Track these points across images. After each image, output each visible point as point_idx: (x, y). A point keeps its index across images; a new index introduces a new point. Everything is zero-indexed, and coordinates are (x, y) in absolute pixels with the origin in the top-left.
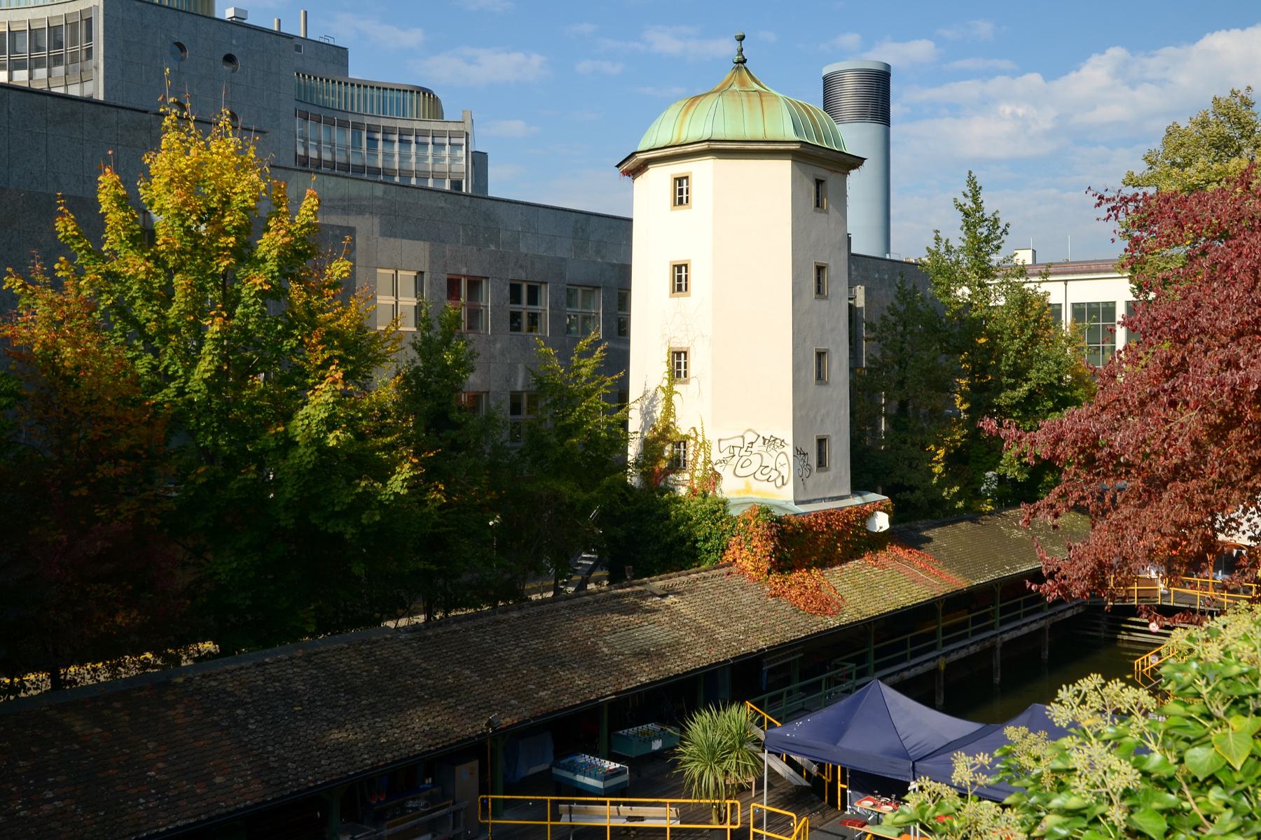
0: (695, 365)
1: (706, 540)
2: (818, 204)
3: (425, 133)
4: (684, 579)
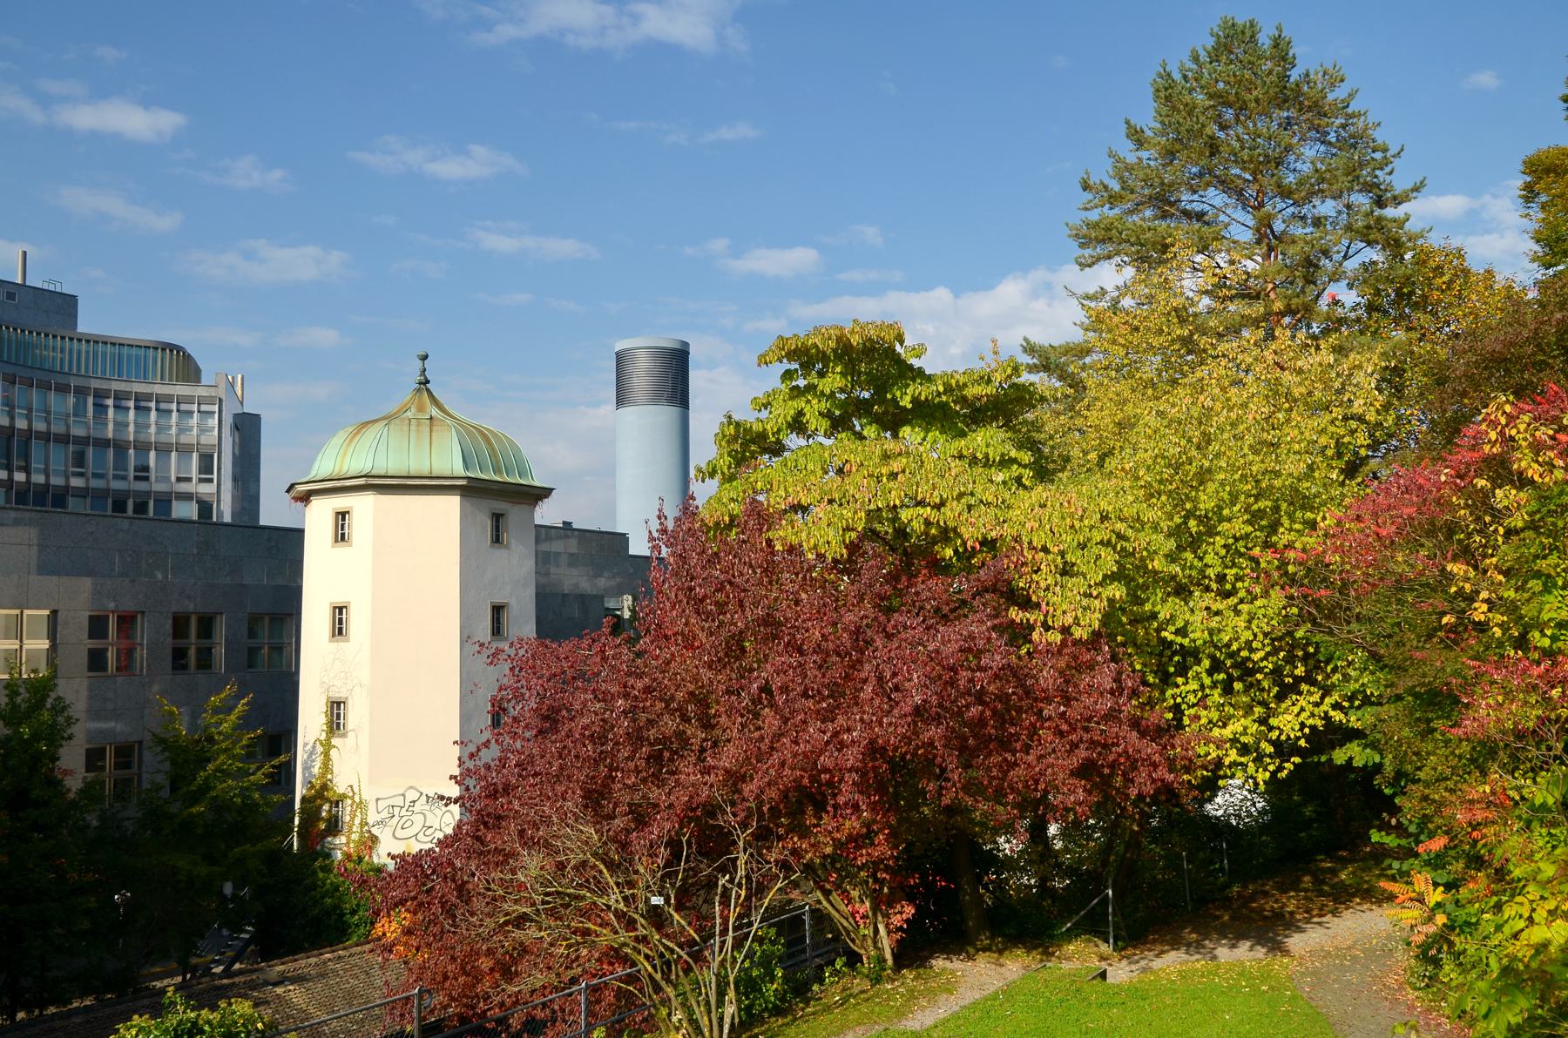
0: (354, 716)
1: (353, 912)
2: (497, 539)
3: (169, 399)
4: (313, 960)
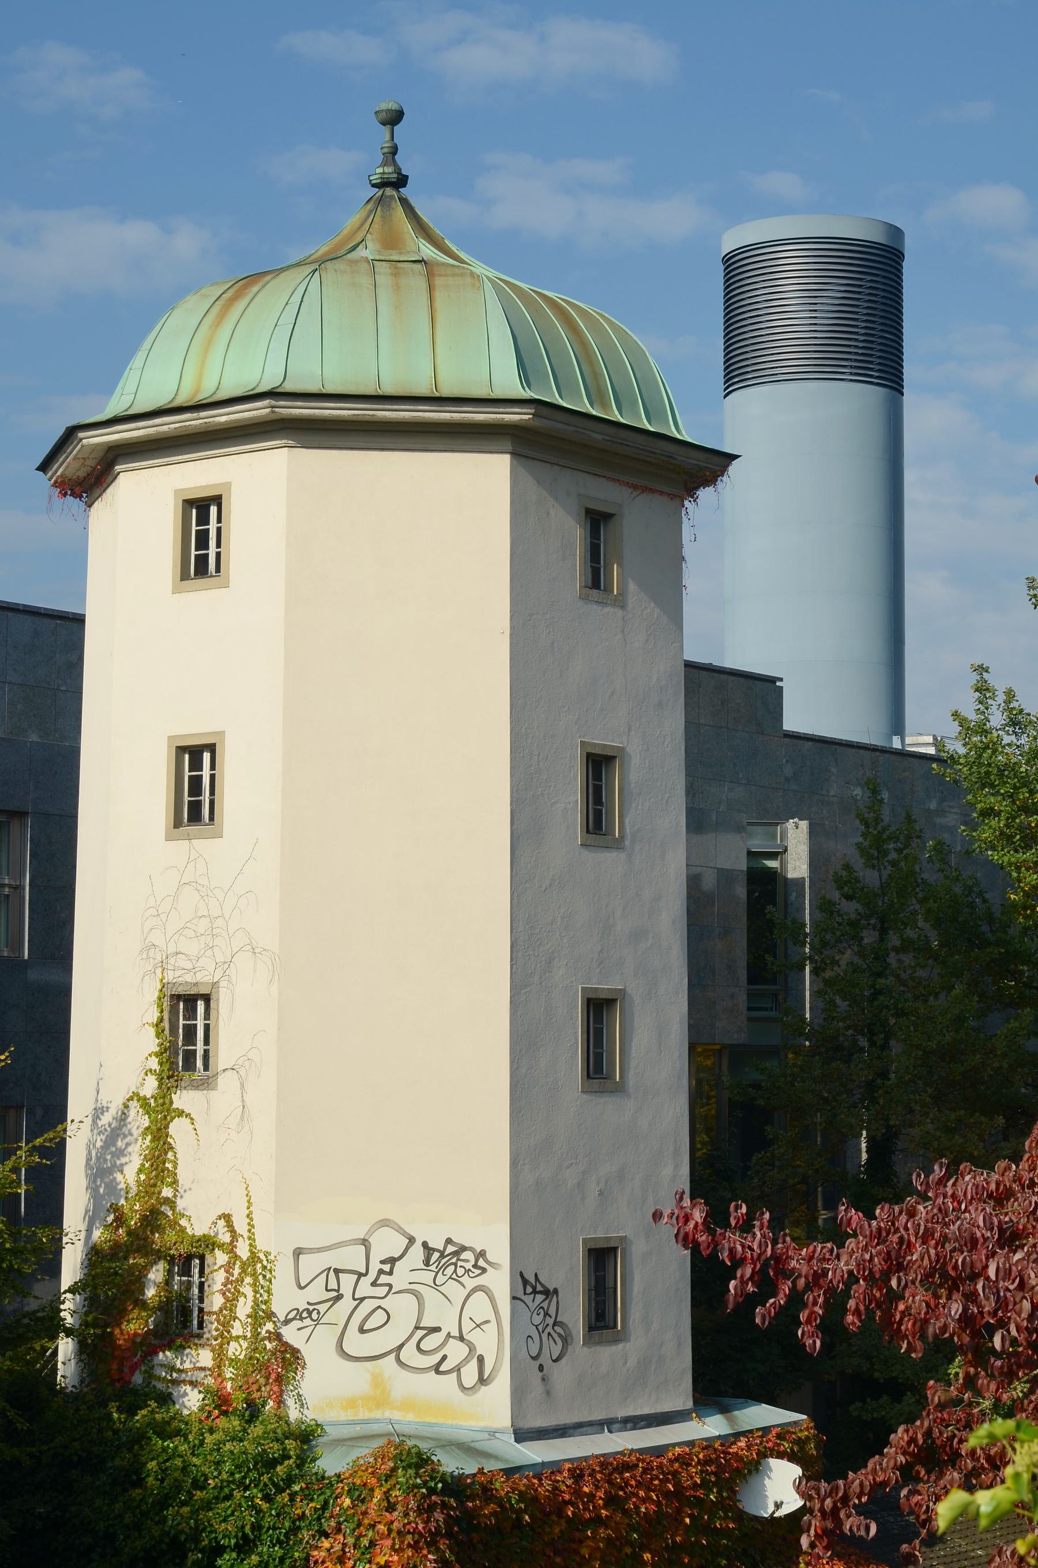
2: (596, 580)
